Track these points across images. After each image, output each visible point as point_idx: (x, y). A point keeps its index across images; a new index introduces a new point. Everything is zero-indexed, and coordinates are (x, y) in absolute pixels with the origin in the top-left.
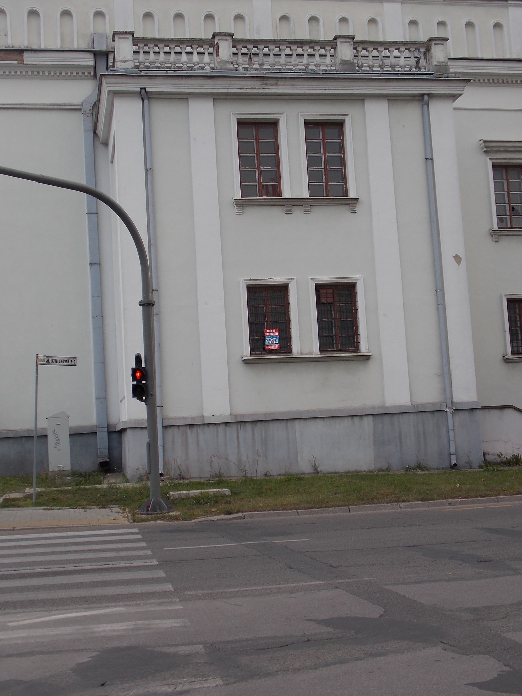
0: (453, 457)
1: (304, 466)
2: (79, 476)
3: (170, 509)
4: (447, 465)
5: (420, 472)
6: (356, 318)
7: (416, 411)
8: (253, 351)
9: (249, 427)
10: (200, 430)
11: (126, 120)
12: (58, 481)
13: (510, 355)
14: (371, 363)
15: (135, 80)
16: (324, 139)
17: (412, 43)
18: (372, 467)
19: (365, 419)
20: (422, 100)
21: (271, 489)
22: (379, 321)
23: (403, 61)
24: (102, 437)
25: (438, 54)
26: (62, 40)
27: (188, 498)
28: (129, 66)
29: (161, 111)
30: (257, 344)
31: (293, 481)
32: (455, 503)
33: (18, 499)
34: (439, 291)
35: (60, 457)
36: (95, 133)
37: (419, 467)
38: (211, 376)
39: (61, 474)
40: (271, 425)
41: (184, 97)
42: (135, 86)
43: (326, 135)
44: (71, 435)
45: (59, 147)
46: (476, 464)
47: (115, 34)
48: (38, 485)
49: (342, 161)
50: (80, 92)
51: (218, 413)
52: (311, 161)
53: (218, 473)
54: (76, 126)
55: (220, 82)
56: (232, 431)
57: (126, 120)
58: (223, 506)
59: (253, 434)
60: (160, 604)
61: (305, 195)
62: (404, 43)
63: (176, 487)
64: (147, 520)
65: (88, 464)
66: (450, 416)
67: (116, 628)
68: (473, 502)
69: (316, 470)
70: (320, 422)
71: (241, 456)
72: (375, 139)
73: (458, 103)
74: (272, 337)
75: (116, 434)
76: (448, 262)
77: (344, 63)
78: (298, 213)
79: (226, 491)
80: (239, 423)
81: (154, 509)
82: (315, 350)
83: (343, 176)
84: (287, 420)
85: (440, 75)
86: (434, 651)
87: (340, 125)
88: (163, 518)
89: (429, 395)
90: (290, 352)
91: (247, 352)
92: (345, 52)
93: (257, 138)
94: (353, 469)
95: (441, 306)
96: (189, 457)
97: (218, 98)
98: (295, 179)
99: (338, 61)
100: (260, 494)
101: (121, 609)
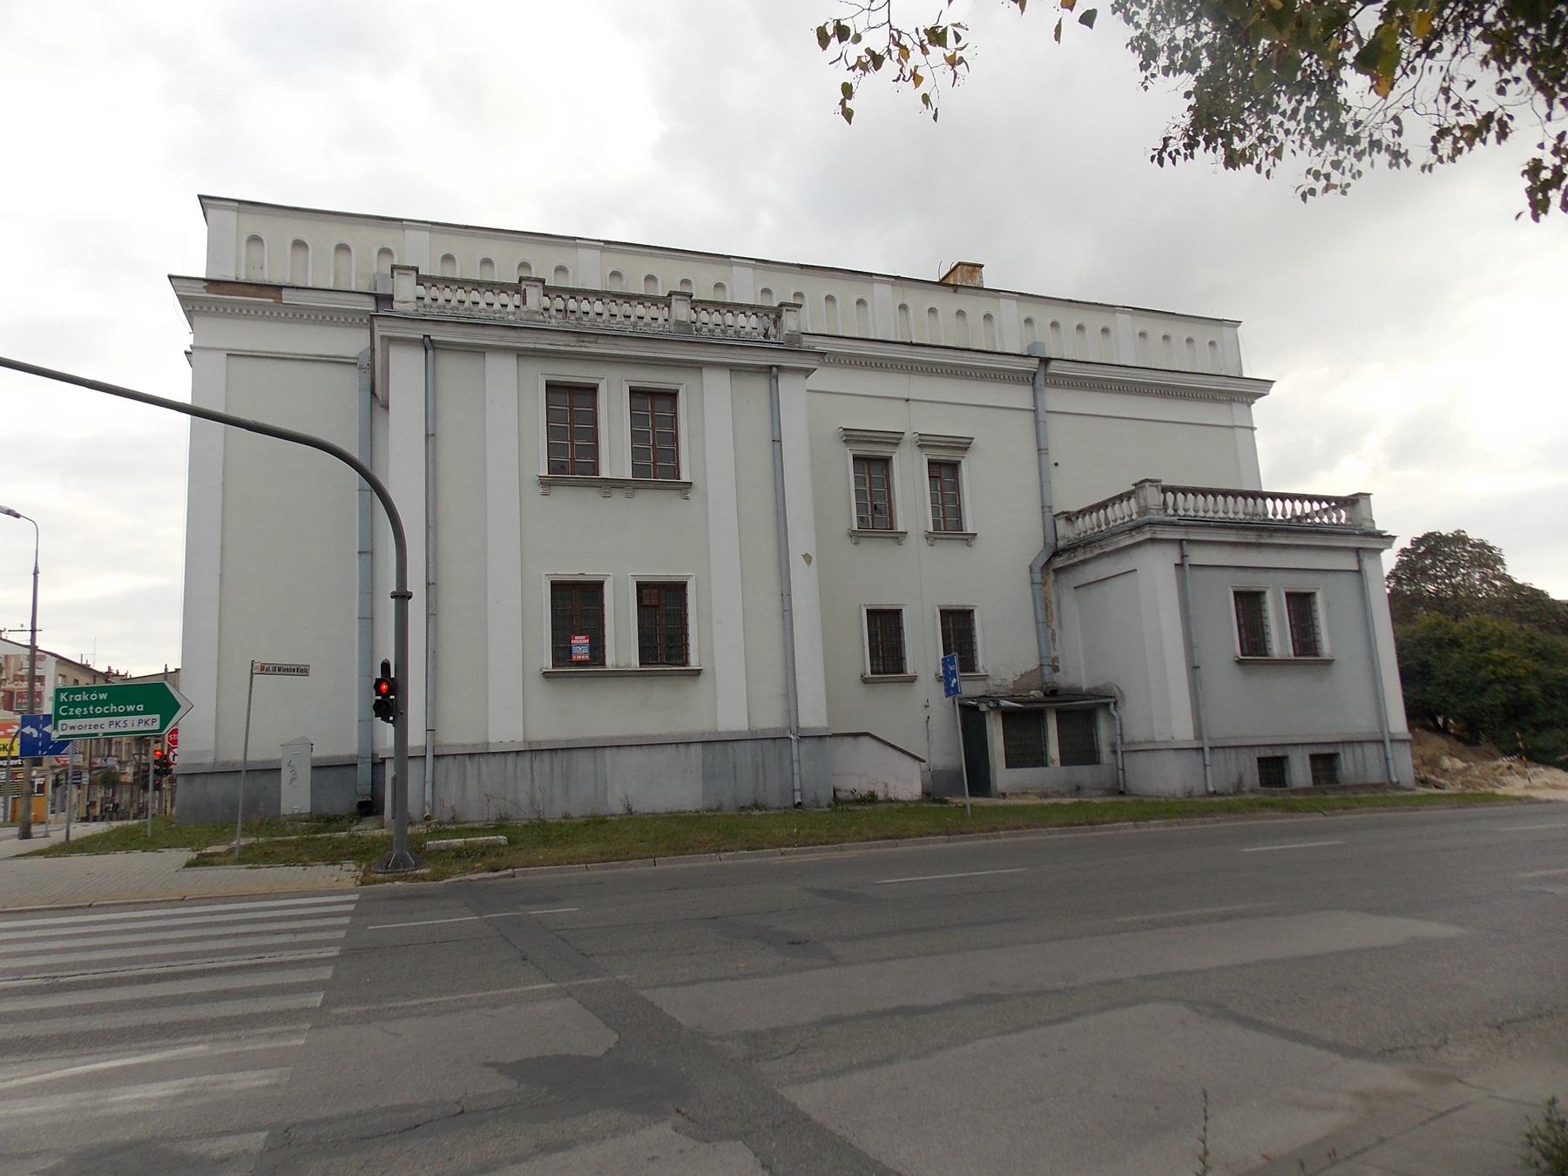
0: (797, 794)
1: (615, 806)
2: (325, 820)
3: (418, 865)
4: (789, 803)
5: (756, 812)
6: (686, 625)
7: (754, 738)
8: (556, 661)
9: (546, 756)
10: (482, 760)
11: (406, 372)
12: (289, 828)
13: (869, 674)
14: (702, 677)
15: (416, 325)
16: (653, 412)
17: (760, 307)
18: (699, 807)
19: (693, 747)
20: (771, 372)
21: (560, 837)
22: (715, 630)
23: (748, 323)
24: (365, 770)
25: (790, 322)
26: (336, 279)
27: (449, 849)
28: (410, 308)
29: (450, 366)
30: (562, 653)
31: (597, 824)
32: (789, 853)
33: (219, 854)
34: (785, 596)
35: (296, 797)
36: (373, 392)
37: (756, 806)
38: (493, 691)
39: (294, 819)
40: (575, 753)
41: (479, 350)
42: (417, 332)
43: (655, 409)
44: (313, 768)
45: (327, 406)
46: (824, 803)
47: (393, 268)
48: (248, 831)
49: (675, 438)
50: (352, 342)
51: (506, 739)
52: (635, 436)
53: (533, 816)
54: (349, 384)
55: (525, 334)
56: (524, 762)
57: (406, 372)
58: (493, 859)
59: (552, 765)
60: (272, 1036)
61: (628, 474)
62: (751, 307)
63: (437, 834)
64: (382, 881)
65: (341, 803)
66: (794, 743)
67: (150, 1094)
68: (810, 852)
69: (629, 811)
70: (637, 752)
71: (526, 792)
72: (713, 414)
73: (815, 381)
74: (580, 646)
75: (378, 764)
76: (796, 562)
77: (679, 323)
78: (618, 497)
79: (502, 839)
80: (534, 751)
81: (396, 866)
82: (634, 663)
83: (675, 455)
84: (595, 748)
85: (792, 345)
86: (660, 1134)
87: (672, 396)
88: (405, 878)
89: (771, 719)
90: (603, 664)
91: (547, 663)
92: (682, 311)
93: (571, 406)
94: (675, 809)
95: (787, 612)
96: (468, 795)
97: (522, 354)
98: (616, 457)
99: (672, 321)
100: (546, 842)
101: (201, 1049)
